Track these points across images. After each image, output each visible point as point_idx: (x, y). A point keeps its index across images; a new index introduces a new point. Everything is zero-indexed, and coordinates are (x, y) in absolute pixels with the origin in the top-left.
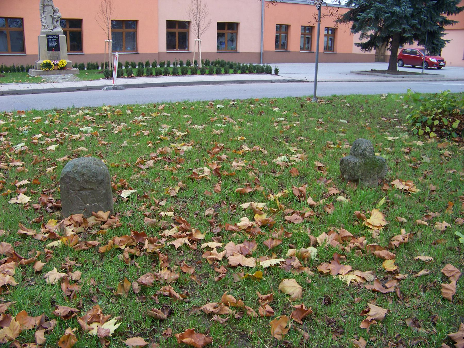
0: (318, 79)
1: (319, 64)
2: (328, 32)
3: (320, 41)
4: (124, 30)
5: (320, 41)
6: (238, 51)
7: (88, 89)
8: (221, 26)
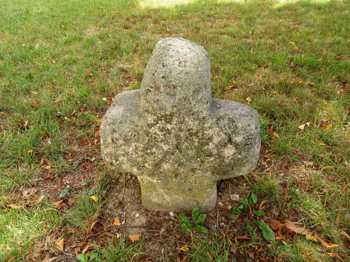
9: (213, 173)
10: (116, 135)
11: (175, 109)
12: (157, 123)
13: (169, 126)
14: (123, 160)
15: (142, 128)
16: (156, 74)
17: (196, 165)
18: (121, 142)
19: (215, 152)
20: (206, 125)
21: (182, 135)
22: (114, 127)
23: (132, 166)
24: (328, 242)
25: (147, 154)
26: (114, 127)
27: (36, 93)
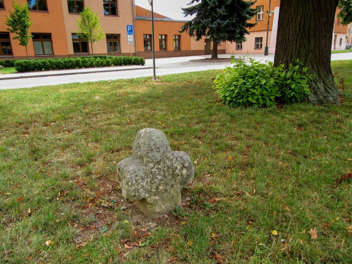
0: (152, 70)
1: (156, 60)
2: (162, 37)
3: (172, 45)
4: (113, 41)
5: (172, 45)
6: (121, 53)
7: (22, 77)
8: (109, 37)
9: (180, 184)
10: (138, 178)
11: (161, 157)
12: (155, 166)
13: (160, 167)
14: (141, 191)
15: (149, 170)
16: (150, 144)
17: (173, 183)
18: (140, 180)
19: (180, 173)
20: (173, 162)
21: (165, 169)
22: (136, 174)
23: (146, 193)
24: (232, 197)
25: (153, 183)
26: (136, 174)
27: (10, 193)
